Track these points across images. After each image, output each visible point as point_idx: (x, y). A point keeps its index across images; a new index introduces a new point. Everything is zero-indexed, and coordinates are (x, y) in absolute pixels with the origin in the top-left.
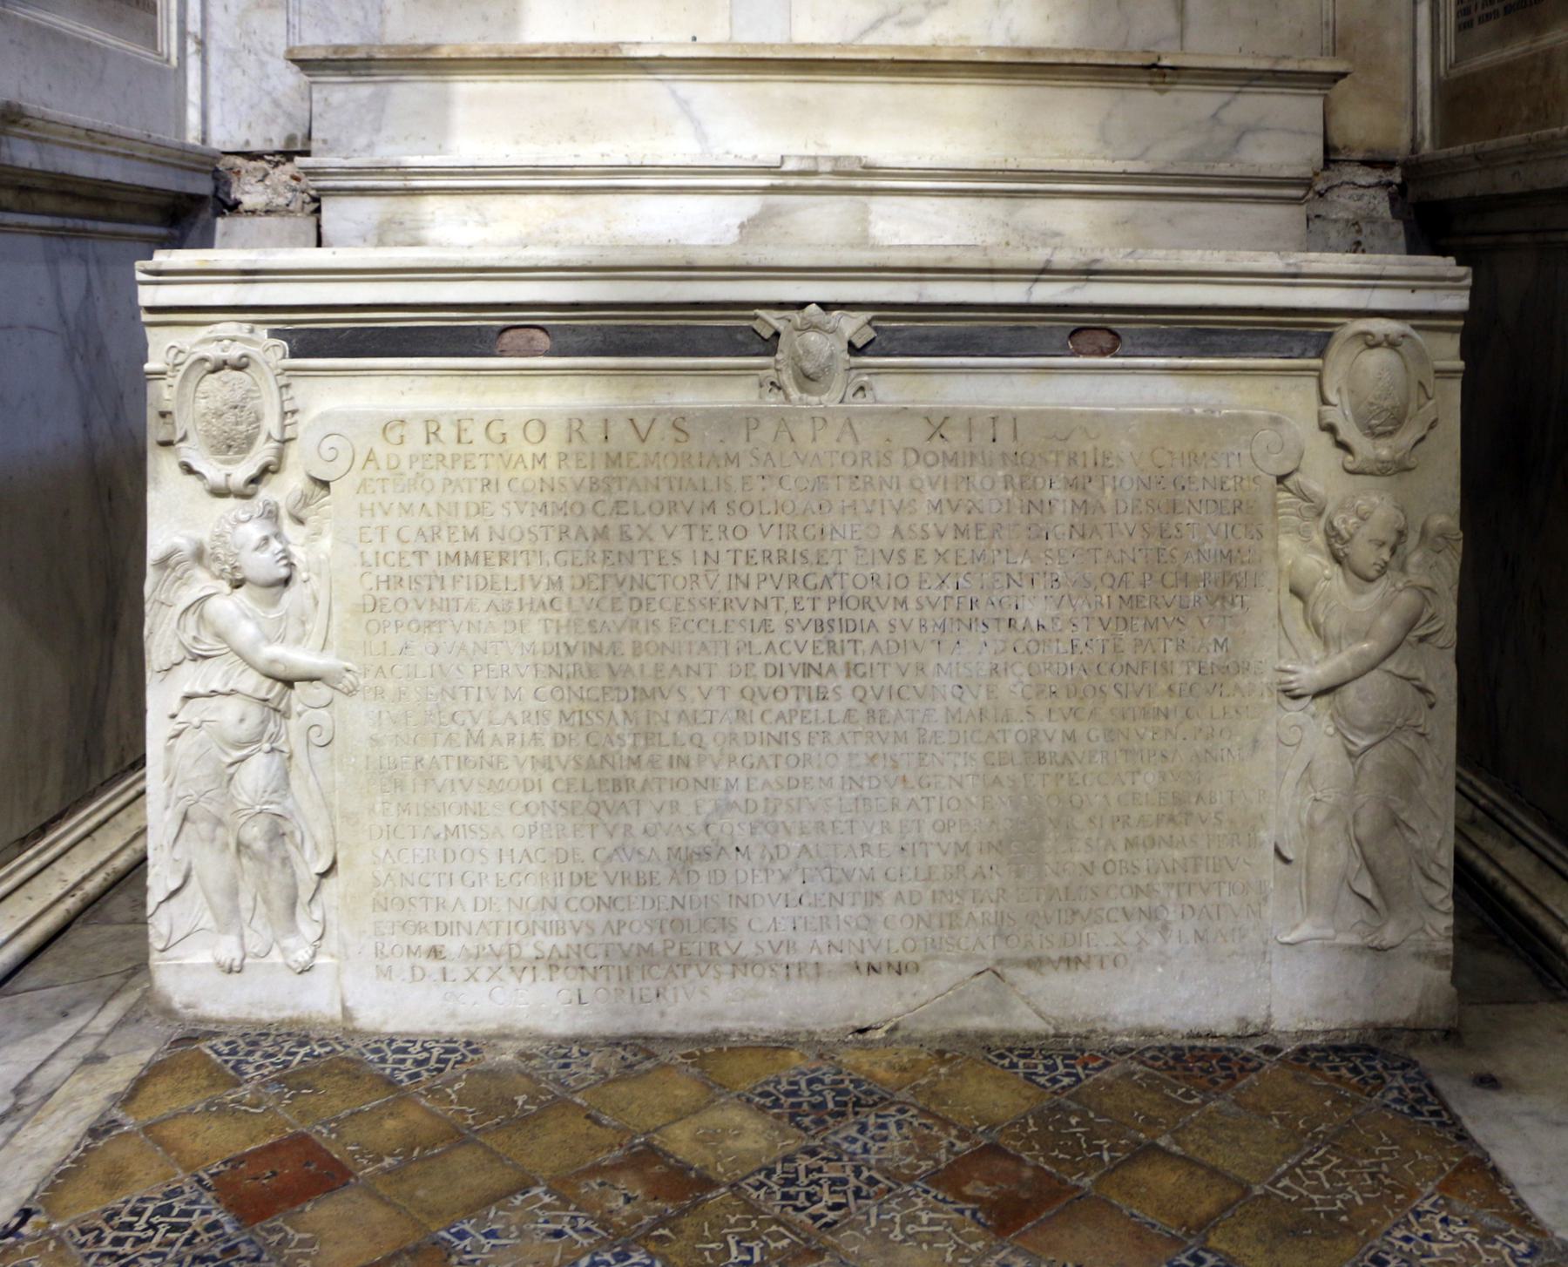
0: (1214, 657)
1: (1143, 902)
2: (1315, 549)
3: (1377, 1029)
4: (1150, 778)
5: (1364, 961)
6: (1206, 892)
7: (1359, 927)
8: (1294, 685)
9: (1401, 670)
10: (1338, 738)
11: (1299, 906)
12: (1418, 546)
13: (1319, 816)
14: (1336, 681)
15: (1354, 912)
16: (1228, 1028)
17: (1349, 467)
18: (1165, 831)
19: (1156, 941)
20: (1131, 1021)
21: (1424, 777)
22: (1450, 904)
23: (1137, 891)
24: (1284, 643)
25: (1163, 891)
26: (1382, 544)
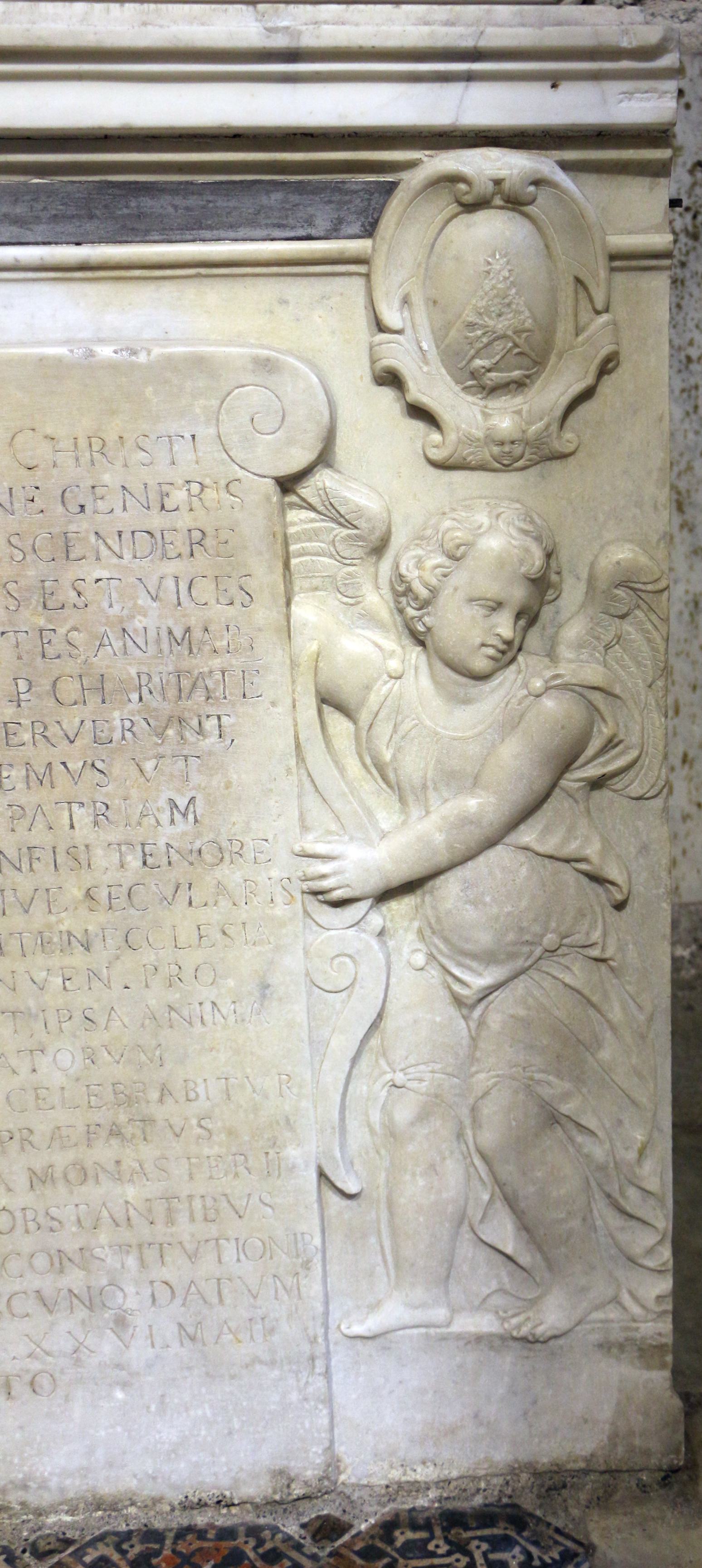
0: (170, 833)
1: (75, 1279)
2: (370, 619)
3: (536, 1474)
4: (65, 1059)
5: (507, 1361)
6: (193, 1257)
7: (497, 1300)
8: (325, 884)
9: (549, 846)
10: (434, 972)
11: (380, 1269)
12: (583, 606)
13: (403, 1114)
14: (360, 896)
15: (483, 1277)
16: (256, 1489)
17: (436, 455)
18: (104, 1152)
19: (107, 1346)
20: (75, 1487)
21: (608, 1034)
22: (666, 1253)
23: (60, 1261)
24: (312, 802)
25: (112, 1260)
26: (497, 606)
